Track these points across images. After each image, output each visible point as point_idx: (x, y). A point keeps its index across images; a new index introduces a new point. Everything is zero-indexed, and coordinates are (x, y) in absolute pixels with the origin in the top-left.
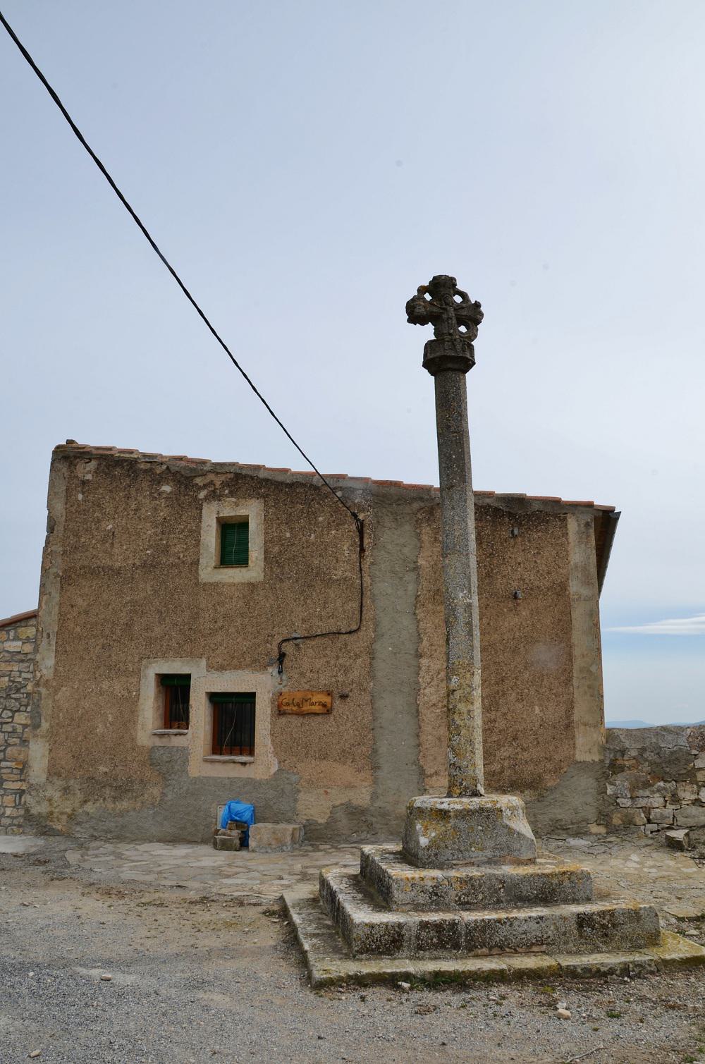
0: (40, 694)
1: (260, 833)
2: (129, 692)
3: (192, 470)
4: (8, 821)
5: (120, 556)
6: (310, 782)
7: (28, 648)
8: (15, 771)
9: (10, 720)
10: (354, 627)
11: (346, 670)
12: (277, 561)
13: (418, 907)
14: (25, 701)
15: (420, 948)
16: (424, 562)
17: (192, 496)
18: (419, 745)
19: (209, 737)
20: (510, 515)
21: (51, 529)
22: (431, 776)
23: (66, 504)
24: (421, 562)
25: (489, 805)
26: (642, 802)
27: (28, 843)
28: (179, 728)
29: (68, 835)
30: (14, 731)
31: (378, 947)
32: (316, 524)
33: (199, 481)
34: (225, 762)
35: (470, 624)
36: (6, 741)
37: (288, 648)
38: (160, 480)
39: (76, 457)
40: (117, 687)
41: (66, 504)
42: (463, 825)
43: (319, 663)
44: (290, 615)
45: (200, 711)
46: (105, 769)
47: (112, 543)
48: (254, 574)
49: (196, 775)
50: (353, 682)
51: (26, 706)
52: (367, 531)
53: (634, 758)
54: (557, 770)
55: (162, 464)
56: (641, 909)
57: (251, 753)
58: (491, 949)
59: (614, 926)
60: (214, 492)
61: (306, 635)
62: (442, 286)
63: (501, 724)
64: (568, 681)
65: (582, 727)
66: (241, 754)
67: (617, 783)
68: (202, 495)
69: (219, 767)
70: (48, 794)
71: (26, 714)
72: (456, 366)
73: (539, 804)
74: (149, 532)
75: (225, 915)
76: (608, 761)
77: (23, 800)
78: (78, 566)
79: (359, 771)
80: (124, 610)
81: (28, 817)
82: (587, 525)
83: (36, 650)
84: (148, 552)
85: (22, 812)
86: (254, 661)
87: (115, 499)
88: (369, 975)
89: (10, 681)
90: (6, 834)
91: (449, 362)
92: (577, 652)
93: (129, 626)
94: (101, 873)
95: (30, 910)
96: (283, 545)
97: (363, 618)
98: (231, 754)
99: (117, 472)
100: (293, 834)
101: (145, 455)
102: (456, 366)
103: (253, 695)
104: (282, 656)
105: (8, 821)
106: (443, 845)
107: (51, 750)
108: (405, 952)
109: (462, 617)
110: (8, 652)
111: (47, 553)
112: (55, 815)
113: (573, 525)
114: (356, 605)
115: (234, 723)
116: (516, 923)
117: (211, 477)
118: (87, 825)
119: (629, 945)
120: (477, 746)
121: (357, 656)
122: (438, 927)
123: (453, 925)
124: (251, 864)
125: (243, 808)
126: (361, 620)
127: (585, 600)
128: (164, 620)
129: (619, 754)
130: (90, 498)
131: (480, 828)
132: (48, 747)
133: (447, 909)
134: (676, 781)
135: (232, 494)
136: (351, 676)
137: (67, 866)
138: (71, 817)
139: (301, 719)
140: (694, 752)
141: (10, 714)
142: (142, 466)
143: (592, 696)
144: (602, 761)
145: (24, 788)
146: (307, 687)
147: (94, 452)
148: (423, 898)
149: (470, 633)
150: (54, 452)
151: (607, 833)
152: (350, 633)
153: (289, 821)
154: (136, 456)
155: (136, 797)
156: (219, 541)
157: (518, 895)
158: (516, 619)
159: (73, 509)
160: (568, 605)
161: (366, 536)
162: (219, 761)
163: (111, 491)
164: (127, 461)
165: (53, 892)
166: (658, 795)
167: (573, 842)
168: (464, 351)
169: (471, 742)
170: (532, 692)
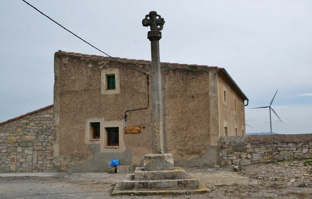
0: (56, 130)
1: (120, 168)
2: (82, 128)
3: (98, 60)
4: (48, 168)
5: (78, 87)
6: (135, 153)
7: (51, 116)
8: (49, 153)
9: (47, 138)
10: (146, 107)
11: (145, 120)
12: (124, 88)
13: (141, 179)
14: (51, 132)
15: (139, 188)
16: (166, 87)
17: (98, 68)
18: (166, 142)
19: (106, 141)
20: (192, 71)
21: (56, 79)
22: (169, 151)
23: (60, 71)
24: (166, 87)
25: (162, 156)
26: (230, 158)
27: (54, 174)
28: (97, 138)
29: (66, 172)
30: (49, 141)
31: (129, 188)
32: (135, 76)
33: (100, 63)
34: (110, 148)
35: (159, 109)
36: (46, 145)
37: (128, 114)
38: (87, 63)
39: (62, 56)
40: (79, 127)
41: (60, 71)
42: (154, 160)
43: (137, 118)
44: (128, 104)
45: (103, 134)
46: (76, 152)
47: (75, 83)
48: (117, 92)
49: (103, 152)
50: (146, 123)
51: (52, 134)
52: (150, 77)
53: (228, 145)
54: (205, 148)
55: (88, 58)
56: (194, 180)
57: (118, 145)
58: (156, 188)
59: (187, 184)
60: (104, 66)
61: (133, 109)
62: (153, 14)
63: (189, 135)
64: (209, 122)
65: (212, 136)
66: (116, 145)
67: (223, 152)
68: (101, 67)
69: (109, 149)
70: (60, 160)
71: (52, 136)
72: (155, 39)
73: (200, 158)
74: (86, 79)
75: (101, 186)
76: (220, 146)
77: (52, 162)
78: (65, 91)
79: (149, 149)
80: (79, 104)
81: (54, 167)
82: (215, 74)
83: (54, 117)
84: (86, 86)
85: (52, 165)
86: (118, 118)
87: (74, 69)
88: (124, 193)
89: (46, 126)
90: (48, 172)
91: (154, 37)
92: (211, 113)
93: (81, 108)
94: (73, 179)
95: (52, 186)
96: (125, 82)
97: (149, 104)
98: (113, 145)
99: (75, 61)
100: (129, 168)
101: (83, 55)
102: (155, 39)
103: (118, 128)
104: (126, 116)
105: (48, 168)
106: (149, 165)
107: (60, 147)
108: (135, 189)
109: (157, 107)
110: (45, 118)
111: (55, 87)
112: (62, 166)
113: (211, 74)
114: (147, 100)
115: (113, 136)
116: (162, 183)
117: (103, 62)
118: (71, 168)
119: (191, 189)
120: (161, 141)
121: (148, 115)
122: (143, 183)
123: (147, 183)
124: (115, 176)
125: (116, 161)
126: (148, 105)
127: (214, 97)
128: (91, 106)
129: (223, 144)
130: (67, 69)
131: (159, 161)
132: (59, 146)
133: (148, 180)
134: (240, 152)
135: (110, 67)
136: (146, 122)
137: (64, 178)
138: (67, 166)
139: (132, 135)
140: (246, 143)
141: (47, 136)
142: (82, 59)
143: (216, 126)
144: (218, 146)
145: (52, 158)
146: (133, 125)
147: (67, 54)
148: (142, 177)
149: (159, 112)
150: (55, 55)
151: (220, 167)
152: (145, 108)
153: (129, 165)
154: (80, 56)
155: (85, 159)
156: (107, 81)
157: (166, 177)
158: (193, 104)
159: (62, 73)
160: (209, 99)
161: (149, 79)
162: (109, 148)
163: (73, 67)
164: (77, 57)
165: (58, 183)
166: (235, 156)
167: (209, 169)
168: (157, 34)
169: (159, 140)
170: (198, 126)
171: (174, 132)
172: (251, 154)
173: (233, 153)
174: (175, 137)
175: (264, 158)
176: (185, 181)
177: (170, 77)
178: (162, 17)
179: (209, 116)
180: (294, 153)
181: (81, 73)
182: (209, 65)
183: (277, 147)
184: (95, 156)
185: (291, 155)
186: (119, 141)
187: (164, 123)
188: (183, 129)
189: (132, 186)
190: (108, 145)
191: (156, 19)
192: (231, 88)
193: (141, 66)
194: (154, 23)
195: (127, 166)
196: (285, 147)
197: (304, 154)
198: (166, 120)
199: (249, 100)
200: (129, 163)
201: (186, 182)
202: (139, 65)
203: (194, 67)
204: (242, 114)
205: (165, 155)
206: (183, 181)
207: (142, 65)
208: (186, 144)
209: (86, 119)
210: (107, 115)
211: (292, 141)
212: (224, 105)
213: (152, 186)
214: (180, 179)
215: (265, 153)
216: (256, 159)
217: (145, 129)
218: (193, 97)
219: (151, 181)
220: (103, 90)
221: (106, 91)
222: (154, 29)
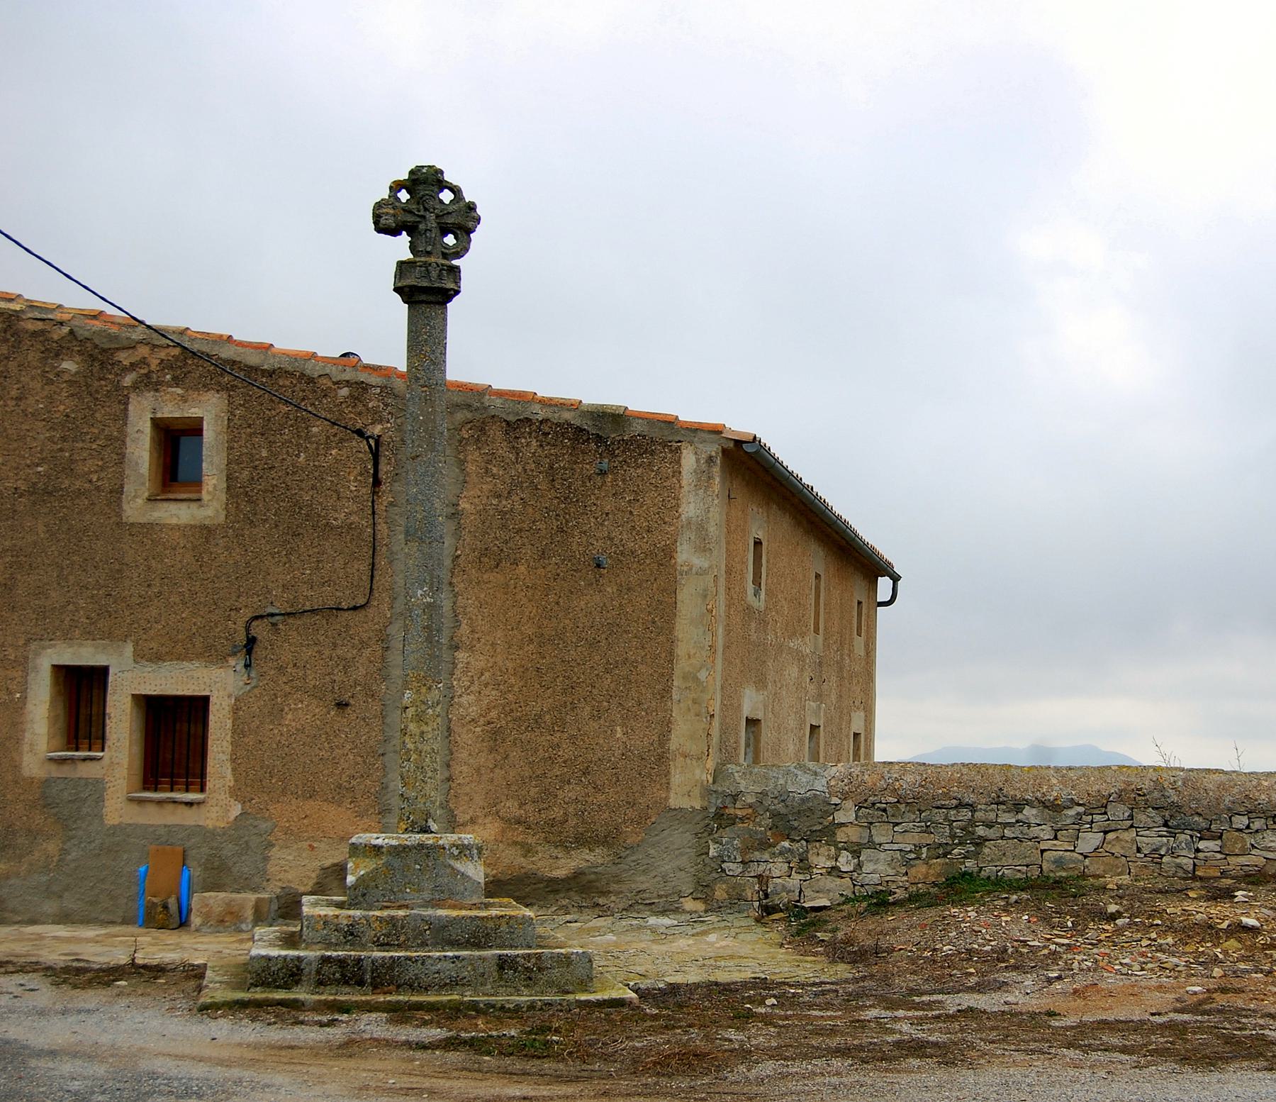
10: (362, 601)
11: (347, 665)
13: (329, 946)
16: (467, 506)
17: (112, 382)
20: (599, 439)
24: (464, 505)
25: (431, 842)
32: (308, 437)
34: (160, 802)
37: (259, 630)
42: (397, 863)
43: (309, 653)
52: (385, 453)
54: (642, 819)
57: (202, 790)
58: (398, 987)
59: (540, 969)
60: (148, 376)
61: (289, 610)
62: (425, 182)
64: (665, 693)
66: (187, 791)
68: (128, 380)
69: (151, 809)
72: (431, 298)
79: (360, 815)
82: (710, 460)
84: (40, 469)
86: (209, 648)
91: (427, 290)
92: (681, 650)
96: (255, 468)
103: (206, 700)
104: (251, 642)
115: (174, 736)
121: (364, 644)
122: (341, 962)
123: (359, 960)
129: (728, 800)
133: (363, 947)
135: (177, 381)
140: (835, 800)
142: (30, 326)
144: (705, 809)
151: (706, 911)
152: (355, 608)
157: (443, 935)
161: (383, 461)
167: (652, 920)
171: (495, 736)
172: (856, 854)
173: (770, 846)
174: (499, 758)
175: (913, 871)
176: (529, 955)
177: (491, 458)
178: (468, 197)
179: (671, 662)
180: (1043, 851)
181: (19, 399)
182: (688, 414)
183: (972, 822)
184: (75, 841)
185: (1027, 861)
186: (209, 769)
187: (453, 695)
188: (538, 719)
189: (292, 974)
190: (145, 789)
191: (441, 202)
192: (799, 524)
193: (345, 392)
194: (428, 218)
195: (243, 895)
196: (1006, 825)
197: (1086, 857)
198: (458, 672)
199: (899, 578)
200: (256, 879)
201: (533, 960)
202: (335, 383)
203: (614, 418)
204: (859, 650)
205: (448, 839)
206: (523, 956)
207: (348, 383)
208: (548, 795)
209: (33, 646)
210: (152, 632)
211: (1039, 795)
212: (749, 607)
213: (383, 977)
214: (511, 947)
215: (918, 847)
216: (875, 878)
217: (349, 710)
218: (598, 566)
219: (378, 954)
220: (136, 497)
221: (150, 505)
222: (429, 253)
